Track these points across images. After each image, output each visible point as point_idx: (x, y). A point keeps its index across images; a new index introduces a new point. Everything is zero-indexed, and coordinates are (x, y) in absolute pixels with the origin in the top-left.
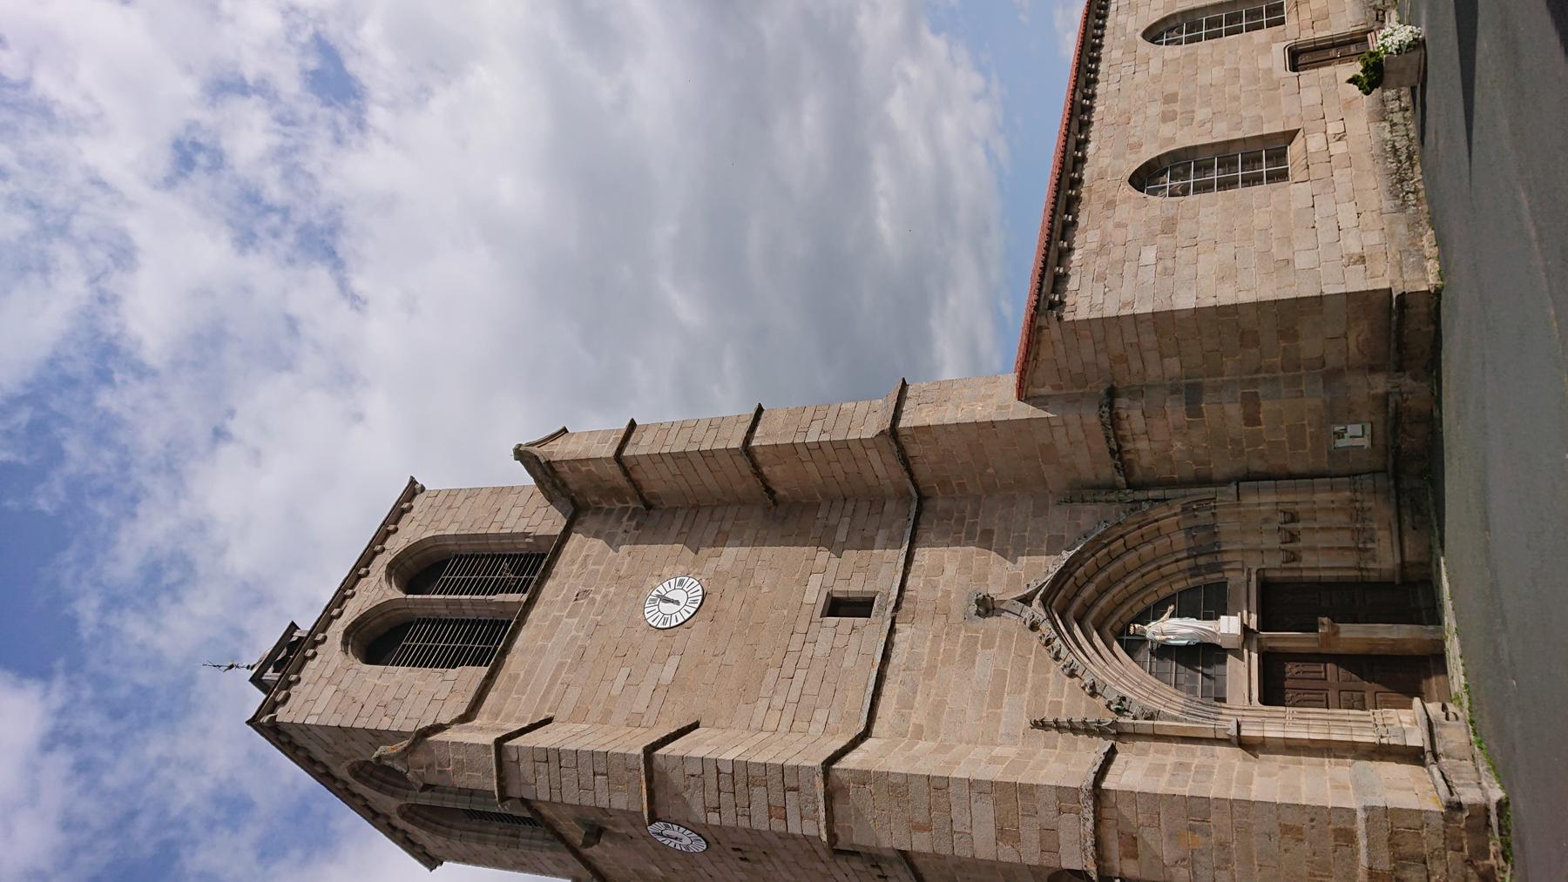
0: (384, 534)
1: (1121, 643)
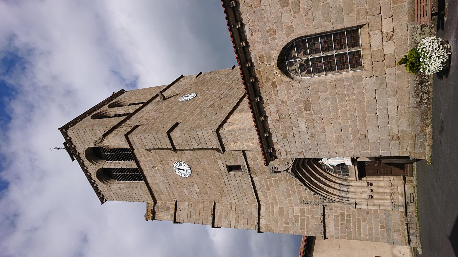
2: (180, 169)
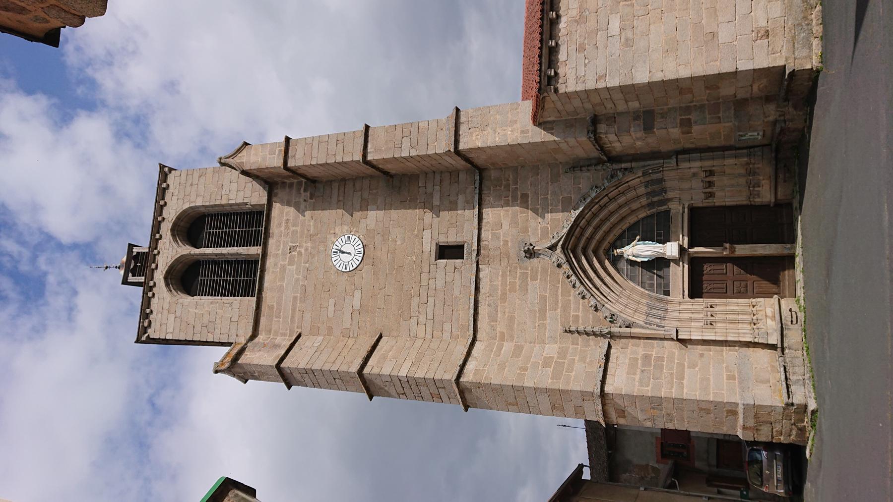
0: (159, 209)
2: (343, 252)
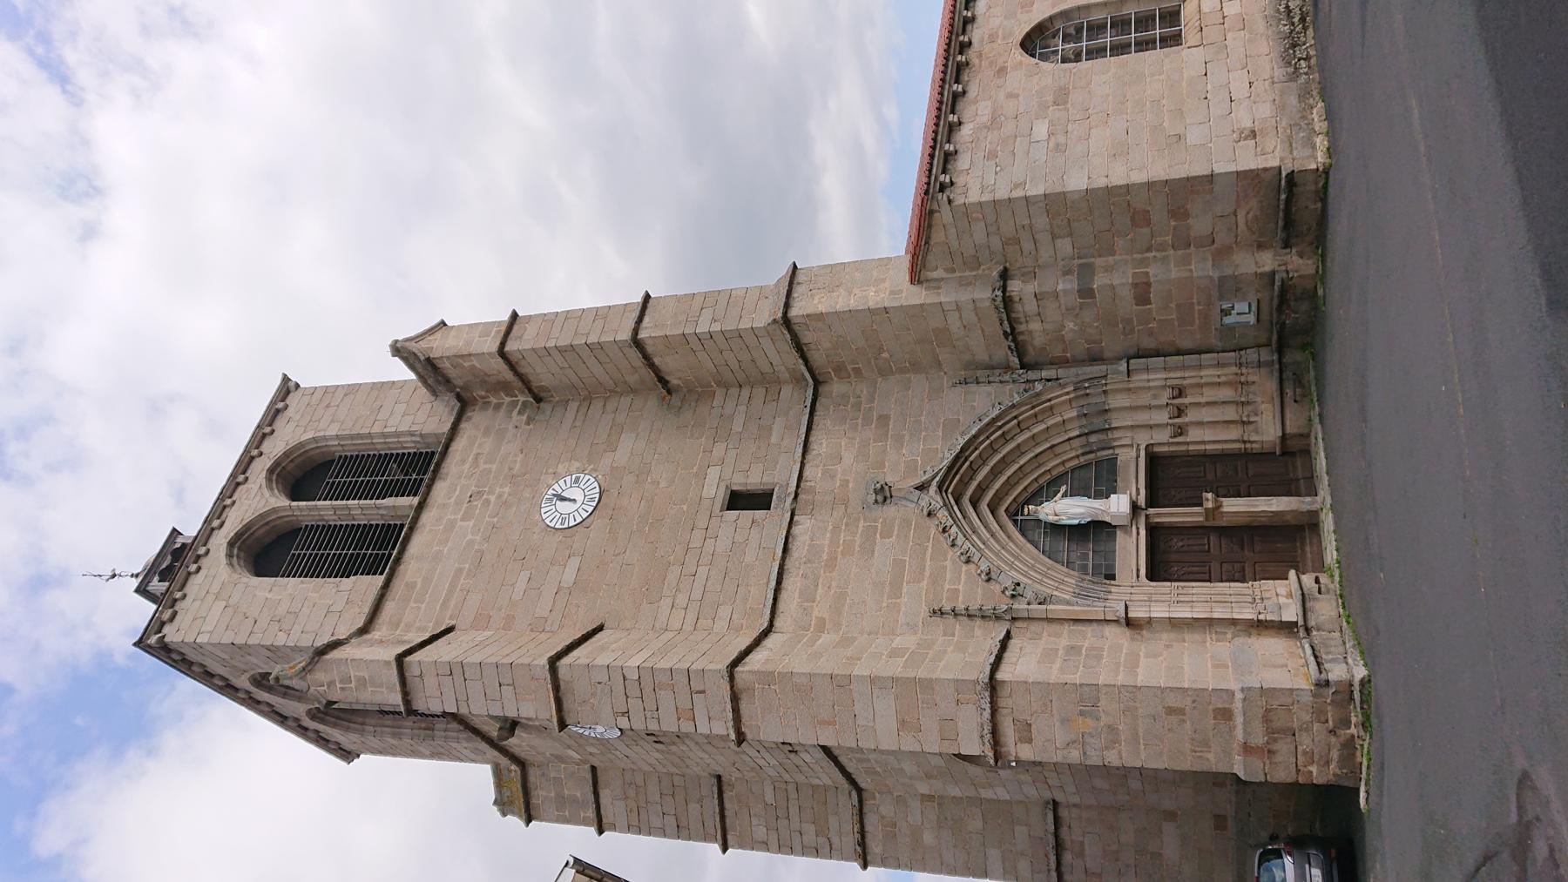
0: (261, 436)
1: (1015, 522)
2: (563, 499)
